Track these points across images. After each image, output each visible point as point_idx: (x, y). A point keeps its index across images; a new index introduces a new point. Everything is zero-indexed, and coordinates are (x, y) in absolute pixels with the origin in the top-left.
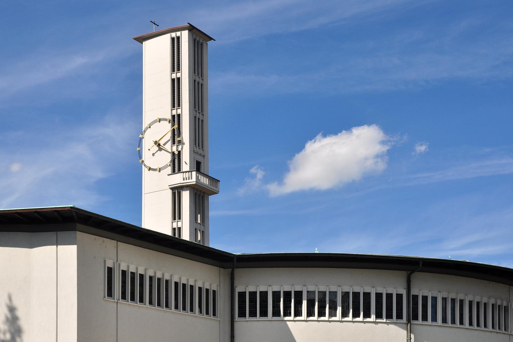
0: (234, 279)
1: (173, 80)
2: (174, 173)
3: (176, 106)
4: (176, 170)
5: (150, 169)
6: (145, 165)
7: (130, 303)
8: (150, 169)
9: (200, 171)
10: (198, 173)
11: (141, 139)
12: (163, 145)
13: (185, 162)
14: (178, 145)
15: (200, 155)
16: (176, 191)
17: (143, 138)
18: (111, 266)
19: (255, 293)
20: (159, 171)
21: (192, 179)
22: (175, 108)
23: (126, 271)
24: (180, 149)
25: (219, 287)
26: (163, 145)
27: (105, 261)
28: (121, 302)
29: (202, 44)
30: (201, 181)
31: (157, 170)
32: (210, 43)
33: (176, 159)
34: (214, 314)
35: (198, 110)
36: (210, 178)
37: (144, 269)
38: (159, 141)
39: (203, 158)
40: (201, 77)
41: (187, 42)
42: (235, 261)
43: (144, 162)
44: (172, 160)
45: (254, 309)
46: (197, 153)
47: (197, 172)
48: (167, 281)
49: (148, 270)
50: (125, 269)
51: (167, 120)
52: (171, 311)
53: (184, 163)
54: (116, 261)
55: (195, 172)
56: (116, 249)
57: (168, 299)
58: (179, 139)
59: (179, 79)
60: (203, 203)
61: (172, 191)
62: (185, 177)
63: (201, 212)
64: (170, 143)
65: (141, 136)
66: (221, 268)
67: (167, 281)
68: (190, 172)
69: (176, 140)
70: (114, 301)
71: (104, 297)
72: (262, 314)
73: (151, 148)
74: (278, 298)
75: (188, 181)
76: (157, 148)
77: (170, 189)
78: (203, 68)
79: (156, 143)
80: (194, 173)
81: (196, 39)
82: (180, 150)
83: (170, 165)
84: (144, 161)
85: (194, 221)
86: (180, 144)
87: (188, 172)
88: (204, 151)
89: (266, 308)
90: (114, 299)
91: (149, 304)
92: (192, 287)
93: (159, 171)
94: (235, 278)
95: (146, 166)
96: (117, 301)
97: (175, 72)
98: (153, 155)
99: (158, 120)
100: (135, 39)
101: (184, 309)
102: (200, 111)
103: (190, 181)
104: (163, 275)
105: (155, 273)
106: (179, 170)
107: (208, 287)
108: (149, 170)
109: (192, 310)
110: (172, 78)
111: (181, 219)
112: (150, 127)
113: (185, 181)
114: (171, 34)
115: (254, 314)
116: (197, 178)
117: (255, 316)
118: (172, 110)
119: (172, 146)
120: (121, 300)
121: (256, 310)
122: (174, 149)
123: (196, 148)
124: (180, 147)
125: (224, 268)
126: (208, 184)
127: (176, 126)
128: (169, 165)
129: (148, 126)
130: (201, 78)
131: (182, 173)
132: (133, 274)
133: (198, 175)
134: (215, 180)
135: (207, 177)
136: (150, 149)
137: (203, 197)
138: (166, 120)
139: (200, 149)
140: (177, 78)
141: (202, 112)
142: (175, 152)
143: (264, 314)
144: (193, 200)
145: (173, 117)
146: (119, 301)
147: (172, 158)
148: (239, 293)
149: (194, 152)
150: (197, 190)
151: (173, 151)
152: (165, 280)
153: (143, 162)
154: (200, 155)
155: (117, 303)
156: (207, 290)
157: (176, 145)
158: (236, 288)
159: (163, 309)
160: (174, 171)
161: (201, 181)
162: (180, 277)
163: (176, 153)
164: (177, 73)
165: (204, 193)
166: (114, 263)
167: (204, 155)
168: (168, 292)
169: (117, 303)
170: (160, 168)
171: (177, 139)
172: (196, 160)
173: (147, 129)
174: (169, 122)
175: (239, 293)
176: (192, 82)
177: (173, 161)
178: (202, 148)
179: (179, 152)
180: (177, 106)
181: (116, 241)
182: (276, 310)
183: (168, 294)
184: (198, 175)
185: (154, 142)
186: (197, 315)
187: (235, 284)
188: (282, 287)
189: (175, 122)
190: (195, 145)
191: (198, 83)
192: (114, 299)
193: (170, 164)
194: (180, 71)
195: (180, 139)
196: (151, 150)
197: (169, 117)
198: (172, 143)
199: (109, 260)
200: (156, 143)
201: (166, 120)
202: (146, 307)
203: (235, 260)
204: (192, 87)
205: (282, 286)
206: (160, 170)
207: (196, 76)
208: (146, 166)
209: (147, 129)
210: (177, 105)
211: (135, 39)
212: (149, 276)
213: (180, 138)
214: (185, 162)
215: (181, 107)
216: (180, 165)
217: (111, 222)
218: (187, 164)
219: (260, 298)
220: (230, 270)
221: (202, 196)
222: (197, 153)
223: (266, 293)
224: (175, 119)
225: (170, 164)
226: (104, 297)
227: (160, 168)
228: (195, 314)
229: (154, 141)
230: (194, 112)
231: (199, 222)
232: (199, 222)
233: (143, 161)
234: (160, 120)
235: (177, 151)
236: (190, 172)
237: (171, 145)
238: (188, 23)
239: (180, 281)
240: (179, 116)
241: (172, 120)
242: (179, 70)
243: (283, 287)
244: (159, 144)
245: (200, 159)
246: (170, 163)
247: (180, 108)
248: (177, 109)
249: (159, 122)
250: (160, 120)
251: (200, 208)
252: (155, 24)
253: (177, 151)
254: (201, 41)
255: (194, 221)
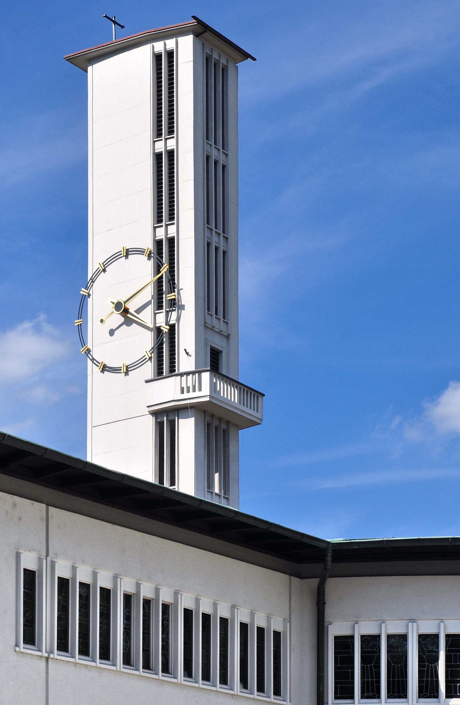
0: (325, 603)
1: (158, 157)
2: (160, 377)
3: (164, 218)
4: (164, 370)
5: (105, 368)
6: (93, 360)
7: (78, 661)
8: (105, 368)
9: (219, 371)
10: (215, 376)
11: (84, 299)
12: (135, 311)
13: (185, 350)
14: (170, 311)
15: (220, 333)
16: (165, 418)
17: (89, 295)
18: (32, 567)
19: (377, 638)
20: (127, 373)
21: (200, 390)
22: (163, 224)
23: (68, 580)
24: (173, 320)
25: (288, 624)
26: (135, 311)
27: (18, 556)
28: (57, 657)
29: (225, 70)
30: (222, 395)
31: (121, 370)
32: (246, 64)
33: (164, 344)
34: (277, 692)
35: (216, 228)
36: (242, 387)
37: (113, 575)
38: (125, 303)
39: (225, 340)
40: (223, 149)
41: (192, 64)
42: (329, 559)
43: (91, 353)
44: (156, 346)
45: (372, 678)
46: (212, 329)
47: (213, 374)
48: (166, 607)
49: (121, 579)
50: (66, 575)
51: (144, 252)
52: (175, 680)
53: (182, 354)
54: (44, 554)
55: (208, 373)
56: (44, 524)
57: (168, 651)
58: (171, 296)
59: (171, 154)
60: (226, 446)
61: (156, 419)
62: (184, 385)
63: (221, 469)
64: (150, 309)
65: (83, 291)
66: (292, 578)
67: (166, 607)
68: (197, 375)
69: (164, 300)
70: (39, 653)
71: (17, 645)
72: (394, 692)
73: (107, 318)
74: (434, 652)
75: (191, 395)
76: (122, 319)
77: (151, 414)
78: (227, 128)
79: (118, 306)
80: (206, 376)
81: (211, 56)
82: (174, 322)
83: (150, 358)
84: (91, 349)
85: (206, 489)
86: (174, 308)
87: (193, 373)
88: (229, 324)
89: (402, 677)
90: (40, 650)
91: (124, 664)
92: (224, 622)
93: (125, 373)
94: (326, 601)
95: (95, 362)
96: (46, 655)
97: (163, 138)
98: (112, 332)
99: (122, 252)
100: (69, 60)
101: (206, 677)
102: (221, 231)
103: (197, 394)
104: (157, 591)
105: (138, 586)
106: (172, 369)
107: (263, 624)
108: (103, 371)
109: (224, 680)
110: (156, 151)
111: (175, 485)
112: (104, 270)
113: (186, 396)
114: (154, 44)
115: (372, 691)
116: (213, 386)
117: (377, 695)
118: (155, 228)
119: (155, 314)
120: (56, 654)
121: (379, 682)
122: (161, 319)
123: (210, 317)
124: (174, 315)
125: (301, 577)
126: (236, 402)
127: (165, 269)
128: (148, 358)
129: (100, 268)
130: (221, 150)
131: (179, 377)
132: (84, 587)
133: (215, 381)
134: (253, 393)
135: (235, 384)
136: (104, 319)
137: (226, 433)
138: (140, 251)
139: (219, 319)
140: (167, 150)
141: (224, 232)
142: (161, 328)
143: (399, 692)
144: (203, 440)
145: (159, 244)
146: (52, 656)
147: (156, 342)
148: (336, 638)
149: (205, 326)
150: (212, 416)
151: (157, 325)
152: (163, 604)
153: (89, 353)
154: (220, 333)
155: (47, 659)
156: (261, 631)
157: (164, 310)
158: (329, 626)
159: (156, 677)
160: (159, 372)
161: (222, 395)
162: (196, 598)
163: (165, 329)
164: (166, 139)
165: (228, 423)
166: (40, 561)
167: (229, 335)
168: (168, 634)
169: (47, 659)
170: (127, 367)
171: (166, 297)
172: (210, 345)
173: (97, 274)
174: (149, 257)
175: (336, 638)
176: (202, 160)
177: (159, 349)
178: (224, 318)
179: (172, 328)
180: (168, 219)
181: (44, 506)
182: (427, 681)
183: (168, 638)
184: (215, 381)
185: (113, 306)
186: (236, 693)
187: (328, 618)
188: (442, 624)
189: (162, 257)
190: (209, 310)
191: (216, 162)
192: (40, 650)
193: (150, 355)
194: (175, 135)
195: (174, 297)
196: (107, 322)
197: (149, 245)
198: (156, 306)
199: (27, 553)
200: (118, 306)
201: (140, 251)
202: (116, 671)
203: (329, 555)
204: (202, 173)
205: (442, 621)
206: (127, 370)
207: (211, 145)
208: (95, 362)
209: (97, 274)
210: (168, 216)
211: (69, 60)
212: (124, 594)
213: (174, 294)
214: (185, 350)
215: (175, 221)
216: (175, 358)
217: (34, 455)
218: (190, 356)
219: (388, 652)
220: (315, 582)
221: (224, 431)
222: (212, 329)
223: (404, 638)
224: (163, 250)
225: (150, 355)
226: (17, 645)
227: (127, 367)
228: (232, 689)
229: (113, 303)
230: (206, 232)
231: (217, 490)
232: (217, 490)
233: (89, 350)
234: (127, 253)
235: (166, 325)
236: (197, 375)
237: (154, 311)
238: (194, 17)
239: (196, 607)
240: (171, 241)
241: (155, 252)
242: (171, 131)
243: (444, 624)
244: (124, 308)
245: (219, 343)
246: (151, 354)
247: (174, 224)
248: (167, 225)
249: (127, 257)
250: (127, 253)
251: (219, 453)
252: (115, 22)
253: (166, 325)
254: (223, 61)
255: (204, 490)
